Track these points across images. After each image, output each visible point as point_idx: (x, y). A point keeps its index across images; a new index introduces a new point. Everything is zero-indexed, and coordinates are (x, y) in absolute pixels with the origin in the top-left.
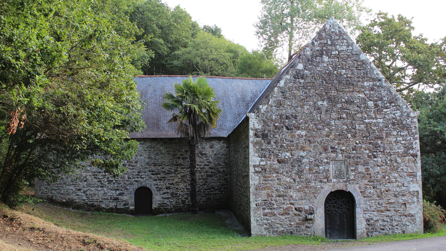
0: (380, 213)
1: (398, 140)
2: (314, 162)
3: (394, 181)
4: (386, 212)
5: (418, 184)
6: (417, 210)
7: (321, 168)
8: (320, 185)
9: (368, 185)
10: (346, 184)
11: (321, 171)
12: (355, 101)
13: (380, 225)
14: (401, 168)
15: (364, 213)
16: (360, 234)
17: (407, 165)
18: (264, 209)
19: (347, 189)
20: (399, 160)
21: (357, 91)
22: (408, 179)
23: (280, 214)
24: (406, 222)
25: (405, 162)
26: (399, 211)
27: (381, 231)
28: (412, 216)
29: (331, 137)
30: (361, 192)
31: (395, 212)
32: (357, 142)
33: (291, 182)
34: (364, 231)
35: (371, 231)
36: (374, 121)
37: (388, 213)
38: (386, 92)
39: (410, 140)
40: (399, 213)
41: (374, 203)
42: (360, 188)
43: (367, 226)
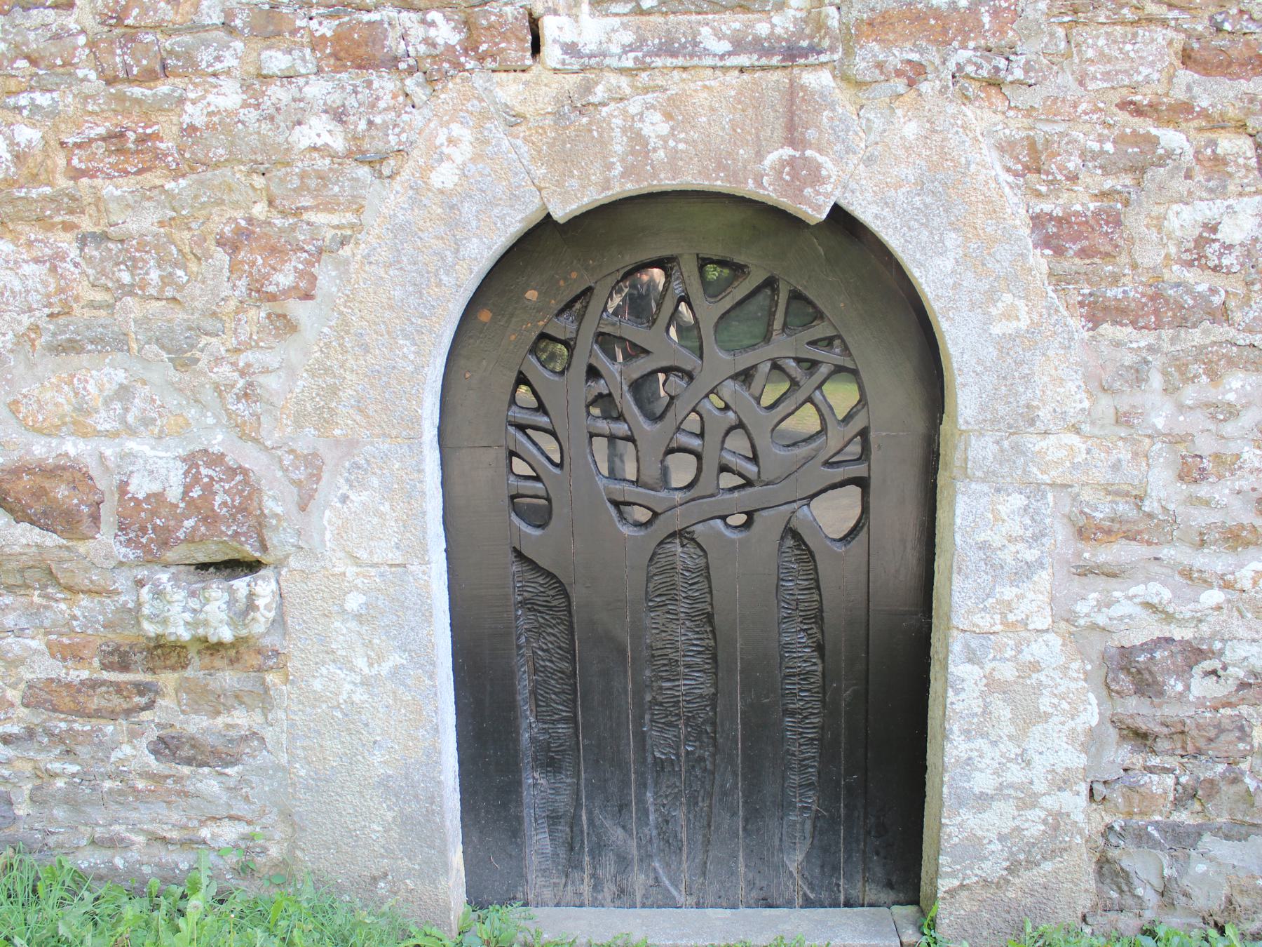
8: (339, 115)
9: (1180, 112)
15: (1086, 571)
16: (993, 868)
43: (1122, 754)
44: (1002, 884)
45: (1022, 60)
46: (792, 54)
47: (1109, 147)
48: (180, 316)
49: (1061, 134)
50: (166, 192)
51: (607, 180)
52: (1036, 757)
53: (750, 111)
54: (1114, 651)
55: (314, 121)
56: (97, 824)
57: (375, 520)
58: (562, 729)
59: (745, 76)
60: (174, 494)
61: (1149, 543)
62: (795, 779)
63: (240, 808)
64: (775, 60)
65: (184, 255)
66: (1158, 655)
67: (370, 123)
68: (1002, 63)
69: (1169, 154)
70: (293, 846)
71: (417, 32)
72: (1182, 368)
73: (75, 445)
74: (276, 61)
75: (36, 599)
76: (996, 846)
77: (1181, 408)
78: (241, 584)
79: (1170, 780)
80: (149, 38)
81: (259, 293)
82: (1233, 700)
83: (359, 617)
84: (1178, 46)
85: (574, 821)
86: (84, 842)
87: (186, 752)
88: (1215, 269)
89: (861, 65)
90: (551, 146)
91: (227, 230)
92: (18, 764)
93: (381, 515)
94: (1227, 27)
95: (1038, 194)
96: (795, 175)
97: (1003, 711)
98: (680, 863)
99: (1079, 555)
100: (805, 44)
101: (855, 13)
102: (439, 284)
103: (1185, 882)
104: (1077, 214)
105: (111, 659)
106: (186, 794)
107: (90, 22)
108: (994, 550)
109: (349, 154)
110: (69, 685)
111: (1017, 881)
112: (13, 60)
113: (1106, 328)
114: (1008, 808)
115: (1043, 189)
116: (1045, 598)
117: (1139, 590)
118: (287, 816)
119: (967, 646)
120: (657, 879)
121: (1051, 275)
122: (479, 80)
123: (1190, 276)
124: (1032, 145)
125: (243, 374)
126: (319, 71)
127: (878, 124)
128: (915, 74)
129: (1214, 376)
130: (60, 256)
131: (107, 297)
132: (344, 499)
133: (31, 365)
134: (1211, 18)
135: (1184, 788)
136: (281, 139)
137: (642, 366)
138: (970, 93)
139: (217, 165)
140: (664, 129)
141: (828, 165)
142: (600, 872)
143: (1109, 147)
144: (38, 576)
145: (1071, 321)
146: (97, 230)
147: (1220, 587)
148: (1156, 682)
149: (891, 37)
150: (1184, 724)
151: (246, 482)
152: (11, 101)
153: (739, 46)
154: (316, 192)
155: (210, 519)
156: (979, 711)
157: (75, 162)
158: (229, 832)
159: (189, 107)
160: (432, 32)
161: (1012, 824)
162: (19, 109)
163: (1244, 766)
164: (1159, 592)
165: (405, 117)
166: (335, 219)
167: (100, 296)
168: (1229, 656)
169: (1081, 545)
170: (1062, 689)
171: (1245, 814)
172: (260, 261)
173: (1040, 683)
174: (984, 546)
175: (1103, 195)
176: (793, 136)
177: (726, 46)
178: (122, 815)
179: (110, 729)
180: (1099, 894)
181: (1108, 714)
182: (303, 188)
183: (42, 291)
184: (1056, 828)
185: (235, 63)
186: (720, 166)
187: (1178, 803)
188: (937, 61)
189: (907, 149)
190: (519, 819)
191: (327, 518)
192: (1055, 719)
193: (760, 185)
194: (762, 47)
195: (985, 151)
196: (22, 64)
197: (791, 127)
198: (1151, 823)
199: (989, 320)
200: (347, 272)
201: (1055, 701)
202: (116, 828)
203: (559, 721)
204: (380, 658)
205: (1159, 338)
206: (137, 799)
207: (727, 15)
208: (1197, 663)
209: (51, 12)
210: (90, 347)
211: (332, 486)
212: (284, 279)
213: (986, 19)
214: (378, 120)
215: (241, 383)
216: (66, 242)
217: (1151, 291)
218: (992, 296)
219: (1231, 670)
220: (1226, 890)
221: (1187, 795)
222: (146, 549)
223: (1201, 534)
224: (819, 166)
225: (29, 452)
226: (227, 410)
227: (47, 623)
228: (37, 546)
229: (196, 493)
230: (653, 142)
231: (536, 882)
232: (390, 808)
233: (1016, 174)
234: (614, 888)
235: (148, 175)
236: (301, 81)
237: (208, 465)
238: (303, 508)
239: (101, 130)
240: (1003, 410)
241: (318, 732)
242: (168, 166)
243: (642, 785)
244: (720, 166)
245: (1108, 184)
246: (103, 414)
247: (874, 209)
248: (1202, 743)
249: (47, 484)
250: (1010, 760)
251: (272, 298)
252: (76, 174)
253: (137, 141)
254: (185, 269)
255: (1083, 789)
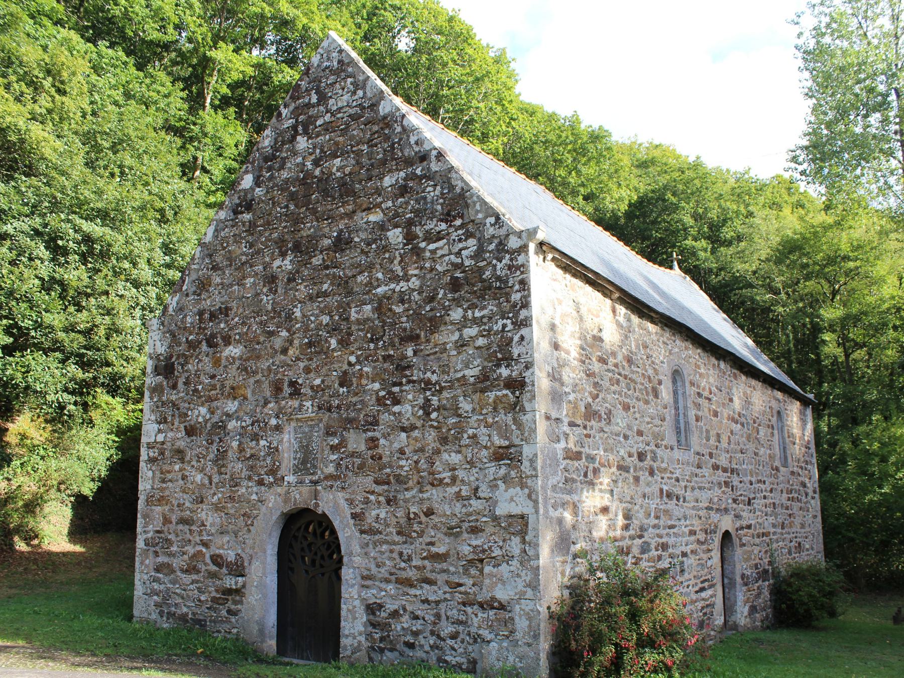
0: (405, 589)
1: (465, 336)
2: (250, 428)
3: (447, 480)
4: (422, 588)
5: (526, 491)
6: (520, 586)
7: (263, 443)
8: (257, 494)
9: (373, 493)
10: (316, 489)
11: (262, 454)
12: (357, 239)
13: (403, 628)
14: (470, 432)
15: (363, 586)
16: (349, 653)
17: (490, 420)
18: (156, 554)
19: (317, 505)
20: (465, 406)
21: (364, 207)
22: (492, 470)
23: (182, 571)
24: (479, 627)
25: (484, 411)
26: (461, 585)
27: (406, 650)
28: (502, 607)
29: (291, 352)
30: (354, 516)
31: (447, 589)
32: (353, 359)
33: (203, 485)
34: (360, 642)
35: (379, 647)
36: (398, 289)
37: (427, 591)
38: (438, 188)
39: (503, 330)
40: (461, 593)
41: (387, 554)
42: (350, 502)
43: (370, 629)
44: (350, 657)
74: (250, 484)
128: (331, 487)
164: (374, 592)
211: (254, 561)
212: (249, 522)
216: (223, 514)
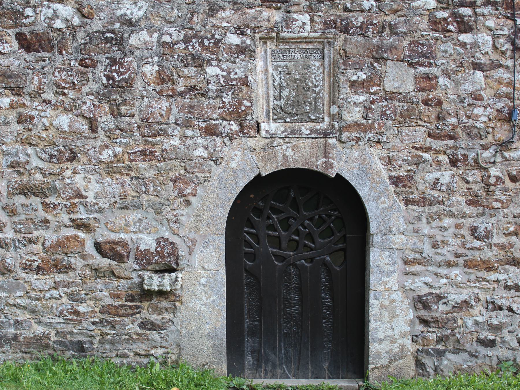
8: (206, 148)
9: (427, 150)
15: (407, 273)
16: (385, 362)
43: (420, 328)
44: (387, 367)
45: (386, 136)
46: (326, 134)
47: (409, 158)
48: (158, 200)
49: (396, 155)
50: (157, 166)
51: (277, 167)
52: (396, 328)
53: (315, 149)
54: (416, 297)
55: (199, 149)
56: (120, 350)
57: (211, 257)
58: (257, 323)
59: (314, 140)
60: (153, 250)
61: (425, 266)
62: (326, 339)
63: (164, 344)
64: (321, 136)
65: (160, 183)
66: (429, 297)
67: (214, 150)
68: (380, 137)
69: (426, 160)
70: (179, 354)
71: (227, 127)
72: (431, 217)
73: (124, 235)
74: (189, 133)
75: (107, 280)
76: (385, 355)
77: (432, 228)
78: (173, 275)
79: (435, 335)
80: (155, 125)
81: (181, 194)
82: (452, 311)
83: (204, 285)
84: (427, 132)
85: (259, 352)
86: (114, 355)
87: (149, 326)
88: (439, 190)
89: (344, 138)
90: (262, 157)
91: (173, 177)
92: (96, 331)
93: (212, 256)
94: (440, 127)
95: (391, 171)
96: (326, 166)
97: (386, 314)
98: (291, 366)
99: (405, 269)
100: (329, 131)
101: (342, 124)
102: (231, 193)
103: (441, 367)
104: (401, 176)
105: (129, 298)
106: (148, 340)
107: (138, 121)
108: (381, 267)
109: (208, 158)
110: (115, 306)
111: (392, 366)
112: (116, 130)
113: (410, 206)
114: (388, 343)
115: (392, 169)
116: (396, 281)
117: (423, 279)
118: (178, 346)
119: (375, 295)
120: (284, 371)
121: (395, 192)
122: (243, 139)
123: (433, 192)
124: (389, 158)
125: (175, 216)
126: (201, 136)
127: (348, 152)
129: (440, 219)
130: (125, 183)
131: (137, 194)
132: (202, 251)
133: (113, 212)
134: (436, 125)
135: (439, 337)
136: (190, 154)
137: (282, 216)
138: (372, 145)
139: (171, 160)
140: (292, 153)
141: (335, 163)
142: (267, 369)
143: (409, 158)
144: (108, 273)
145: (400, 204)
146: (136, 176)
147: (446, 278)
148: (429, 306)
149: (351, 130)
150: (438, 318)
151: (174, 246)
152: (115, 140)
153: (312, 131)
154: (199, 168)
155: (162, 256)
156: (379, 314)
157: (131, 157)
158: (160, 352)
159: (165, 144)
160: (232, 127)
161: (389, 348)
162: (116, 143)
163: (456, 331)
164: (429, 280)
165: (224, 149)
166: (203, 175)
167: (135, 194)
168: (449, 298)
169: (406, 266)
170: (402, 307)
171: (458, 346)
172: (182, 186)
173: (396, 306)
174: (378, 266)
175: (408, 171)
176: (326, 156)
177: (308, 132)
178: (127, 346)
179: (126, 319)
180: (417, 371)
181: (416, 315)
182: (195, 167)
183: (119, 192)
184: (402, 349)
185: (178, 133)
186: (307, 163)
187: (438, 342)
188: (363, 137)
189: (356, 159)
190: (243, 351)
191: (196, 258)
192: (400, 317)
193: (317, 168)
194: (317, 132)
195: (376, 160)
196: (118, 131)
197: (325, 153)
198: (431, 348)
199: (378, 204)
200: (206, 189)
201: (400, 311)
202: (125, 351)
203: (256, 321)
204: (210, 297)
205: (425, 209)
206: (132, 341)
207: (308, 124)
208: (440, 300)
209: (128, 118)
210: (131, 208)
211: (198, 248)
212: (188, 191)
213: (376, 126)
214: (217, 149)
215: (174, 219)
217: (422, 196)
218: (379, 198)
219: (450, 302)
220: (453, 370)
221: (440, 340)
222: (143, 265)
223: (439, 263)
224: (333, 163)
225: (109, 237)
226: (170, 226)
227: (110, 287)
228: (110, 264)
229: (159, 249)
230: (289, 157)
231: (247, 372)
232: (210, 342)
233: (385, 166)
234: (271, 374)
235: (152, 162)
236: (196, 138)
237: (163, 241)
238: (190, 254)
239: (140, 149)
240: (382, 228)
241: (190, 320)
242: (158, 160)
243: (280, 341)
244: (307, 163)
245: (410, 168)
246: (133, 227)
247: (347, 175)
248: (443, 324)
249: (114, 247)
250: (388, 329)
251: (185, 196)
252: (131, 161)
253: (149, 153)
254: (160, 187)
255: (410, 338)
